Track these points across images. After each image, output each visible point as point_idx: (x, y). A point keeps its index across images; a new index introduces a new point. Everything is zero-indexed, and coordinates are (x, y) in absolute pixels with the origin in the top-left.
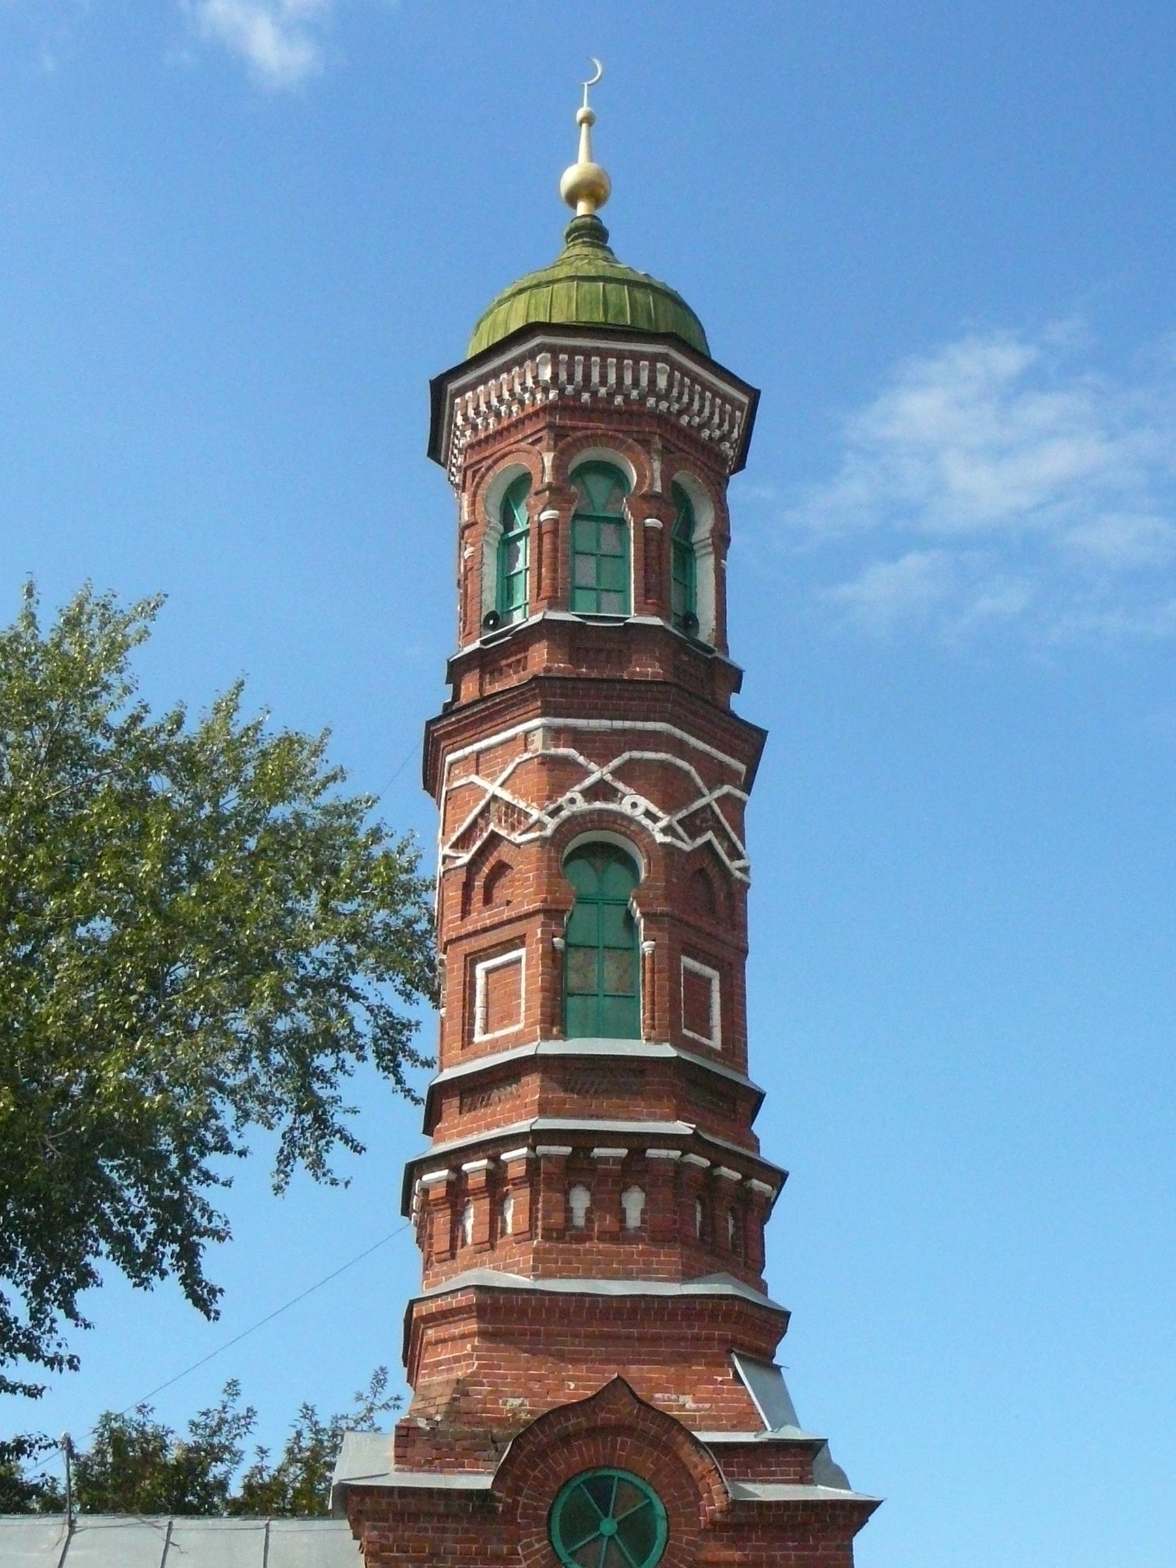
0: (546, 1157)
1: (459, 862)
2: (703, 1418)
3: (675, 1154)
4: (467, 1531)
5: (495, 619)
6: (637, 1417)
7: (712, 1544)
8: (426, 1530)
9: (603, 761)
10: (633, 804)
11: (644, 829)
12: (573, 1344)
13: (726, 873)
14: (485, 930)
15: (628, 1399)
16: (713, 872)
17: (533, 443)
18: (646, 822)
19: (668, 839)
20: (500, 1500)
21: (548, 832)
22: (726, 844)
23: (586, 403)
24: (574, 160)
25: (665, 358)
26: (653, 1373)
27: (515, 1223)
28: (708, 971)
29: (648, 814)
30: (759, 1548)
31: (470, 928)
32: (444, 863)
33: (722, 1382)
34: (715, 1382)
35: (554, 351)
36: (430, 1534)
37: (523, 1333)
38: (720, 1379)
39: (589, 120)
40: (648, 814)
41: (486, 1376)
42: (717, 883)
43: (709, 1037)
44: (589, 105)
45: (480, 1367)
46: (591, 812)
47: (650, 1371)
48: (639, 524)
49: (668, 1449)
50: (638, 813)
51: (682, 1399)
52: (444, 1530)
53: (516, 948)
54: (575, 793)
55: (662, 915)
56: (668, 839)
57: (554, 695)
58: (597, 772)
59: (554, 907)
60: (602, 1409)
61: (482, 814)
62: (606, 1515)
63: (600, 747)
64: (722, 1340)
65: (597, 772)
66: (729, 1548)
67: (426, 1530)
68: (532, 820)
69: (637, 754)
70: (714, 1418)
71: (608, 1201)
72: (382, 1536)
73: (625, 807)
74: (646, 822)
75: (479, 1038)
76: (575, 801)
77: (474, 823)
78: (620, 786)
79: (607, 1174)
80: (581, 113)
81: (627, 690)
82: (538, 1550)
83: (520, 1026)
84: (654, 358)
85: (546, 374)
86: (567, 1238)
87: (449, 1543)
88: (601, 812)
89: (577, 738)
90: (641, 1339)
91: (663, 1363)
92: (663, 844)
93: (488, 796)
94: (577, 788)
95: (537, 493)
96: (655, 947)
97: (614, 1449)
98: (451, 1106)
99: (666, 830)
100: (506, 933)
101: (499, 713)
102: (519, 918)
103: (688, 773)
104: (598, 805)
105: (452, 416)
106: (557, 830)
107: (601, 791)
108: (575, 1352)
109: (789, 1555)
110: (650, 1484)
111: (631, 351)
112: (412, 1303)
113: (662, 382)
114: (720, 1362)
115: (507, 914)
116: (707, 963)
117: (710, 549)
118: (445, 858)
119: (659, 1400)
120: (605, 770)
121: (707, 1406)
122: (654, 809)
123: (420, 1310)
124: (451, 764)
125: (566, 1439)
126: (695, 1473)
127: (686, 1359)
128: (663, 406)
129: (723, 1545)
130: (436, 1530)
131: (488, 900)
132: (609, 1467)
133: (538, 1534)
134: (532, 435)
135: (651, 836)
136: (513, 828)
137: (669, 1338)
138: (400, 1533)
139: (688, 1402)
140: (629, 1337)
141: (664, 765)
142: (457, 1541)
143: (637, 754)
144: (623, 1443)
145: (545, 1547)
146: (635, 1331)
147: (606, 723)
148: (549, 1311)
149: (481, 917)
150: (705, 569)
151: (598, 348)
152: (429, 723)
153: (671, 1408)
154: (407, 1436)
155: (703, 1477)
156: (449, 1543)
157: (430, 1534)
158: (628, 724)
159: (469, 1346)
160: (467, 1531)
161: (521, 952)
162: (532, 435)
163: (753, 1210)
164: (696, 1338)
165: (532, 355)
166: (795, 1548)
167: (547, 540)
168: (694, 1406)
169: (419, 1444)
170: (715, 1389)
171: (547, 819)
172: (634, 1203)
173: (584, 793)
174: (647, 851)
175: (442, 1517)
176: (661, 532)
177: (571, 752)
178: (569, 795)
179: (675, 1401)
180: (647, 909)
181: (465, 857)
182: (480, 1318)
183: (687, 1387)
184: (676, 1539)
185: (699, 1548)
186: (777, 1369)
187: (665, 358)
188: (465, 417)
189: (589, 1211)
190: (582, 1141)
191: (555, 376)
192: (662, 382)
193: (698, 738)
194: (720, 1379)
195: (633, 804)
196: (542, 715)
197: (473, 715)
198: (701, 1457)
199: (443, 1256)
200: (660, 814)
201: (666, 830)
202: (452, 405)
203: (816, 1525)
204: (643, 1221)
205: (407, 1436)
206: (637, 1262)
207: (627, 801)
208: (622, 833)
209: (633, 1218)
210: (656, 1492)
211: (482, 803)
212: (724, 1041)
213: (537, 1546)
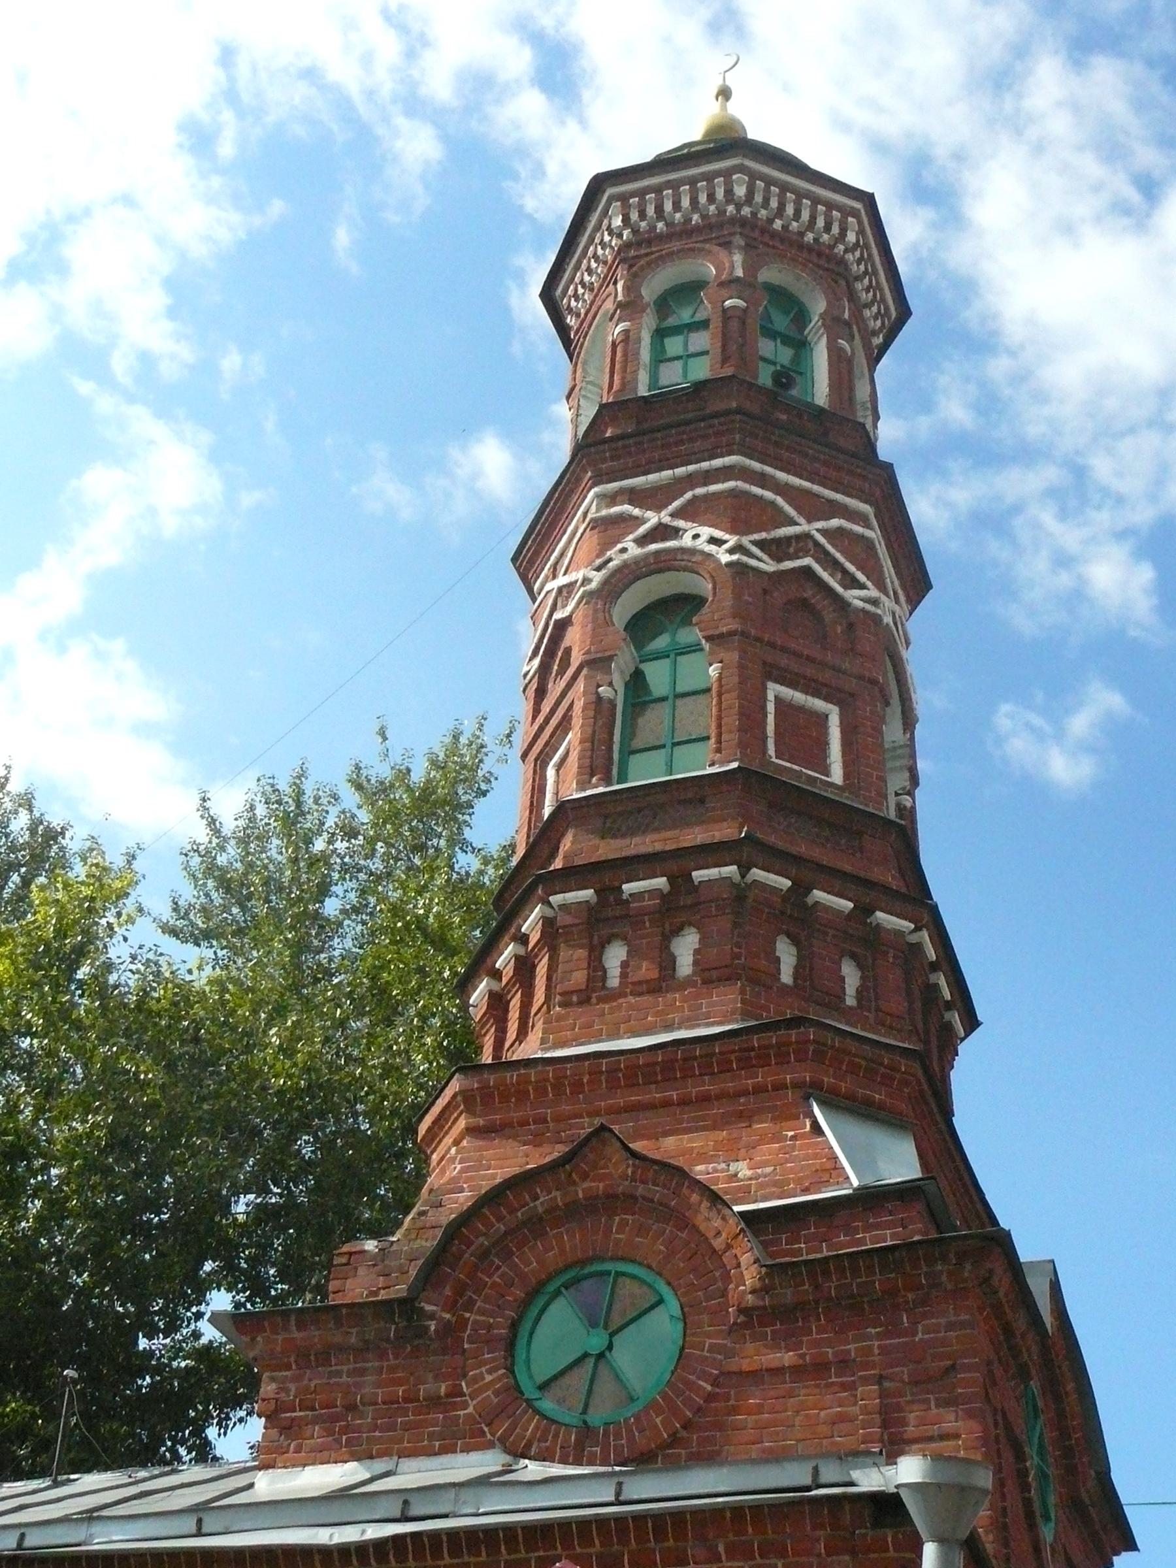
0: (563, 907)
2: (761, 1186)
3: (731, 870)
4: (392, 1369)
6: (633, 1180)
7: (750, 1347)
9: (659, 508)
10: (697, 536)
11: (709, 556)
13: (842, 605)
15: (618, 1155)
16: (818, 601)
18: (712, 549)
20: (432, 1316)
21: (593, 585)
22: (839, 576)
23: (661, 233)
25: (741, 169)
26: (695, 1141)
28: (819, 704)
29: (713, 541)
30: (817, 1344)
33: (793, 1138)
34: (785, 1138)
36: (345, 1379)
37: (523, 1123)
38: (791, 1134)
40: (713, 541)
42: (829, 615)
43: (826, 771)
45: (462, 1171)
46: (646, 556)
47: (691, 1140)
49: (684, 1222)
50: (702, 544)
51: (734, 1167)
52: (362, 1372)
54: (628, 543)
55: (731, 634)
56: (735, 557)
57: (604, 460)
58: (652, 518)
59: (599, 655)
60: (585, 1176)
64: (796, 1085)
65: (652, 518)
66: (776, 1347)
70: (775, 1184)
72: (280, 1390)
73: (686, 541)
78: (681, 523)
79: (642, 912)
81: (684, 433)
84: (727, 174)
85: (740, 191)
86: (594, 1000)
87: (370, 1387)
88: (657, 553)
89: (635, 497)
90: (684, 1102)
91: (714, 1128)
92: (730, 565)
94: (631, 537)
96: (722, 668)
97: (608, 1231)
101: (562, 510)
103: (773, 503)
104: (654, 547)
106: (606, 582)
107: (662, 532)
109: (870, 1347)
110: (660, 1274)
111: (702, 173)
114: (797, 1112)
116: (816, 694)
119: (701, 1173)
120: (663, 514)
121: (769, 1169)
122: (718, 534)
125: (536, 1226)
126: (718, 1243)
127: (746, 1117)
129: (766, 1346)
132: (602, 1259)
133: (493, 1360)
135: (718, 561)
138: (305, 1382)
139: (743, 1169)
140: (667, 1104)
141: (733, 493)
142: (378, 1385)
147: (667, 473)
148: (558, 1087)
151: (669, 181)
152: (514, 560)
153: (716, 1181)
154: (348, 1264)
155: (729, 1247)
156: (370, 1387)
158: (691, 468)
160: (392, 1369)
163: (886, 953)
164: (759, 1090)
167: (619, 349)
168: (749, 1173)
169: (361, 1271)
170: (780, 1149)
173: (636, 541)
174: (712, 577)
175: (360, 1352)
176: (745, 310)
179: (722, 1171)
180: (710, 633)
182: (470, 1110)
183: (743, 1151)
185: (730, 1354)
187: (741, 169)
193: (788, 472)
194: (791, 1134)
195: (697, 536)
196: (595, 485)
198: (724, 1219)
200: (727, 537)
203: (910, 1296)
205: (348, 1264)
208: (685, 569)
209: (685, 965)
210: (669, 1284)
212: (846, 776)
213: (488, 1378)
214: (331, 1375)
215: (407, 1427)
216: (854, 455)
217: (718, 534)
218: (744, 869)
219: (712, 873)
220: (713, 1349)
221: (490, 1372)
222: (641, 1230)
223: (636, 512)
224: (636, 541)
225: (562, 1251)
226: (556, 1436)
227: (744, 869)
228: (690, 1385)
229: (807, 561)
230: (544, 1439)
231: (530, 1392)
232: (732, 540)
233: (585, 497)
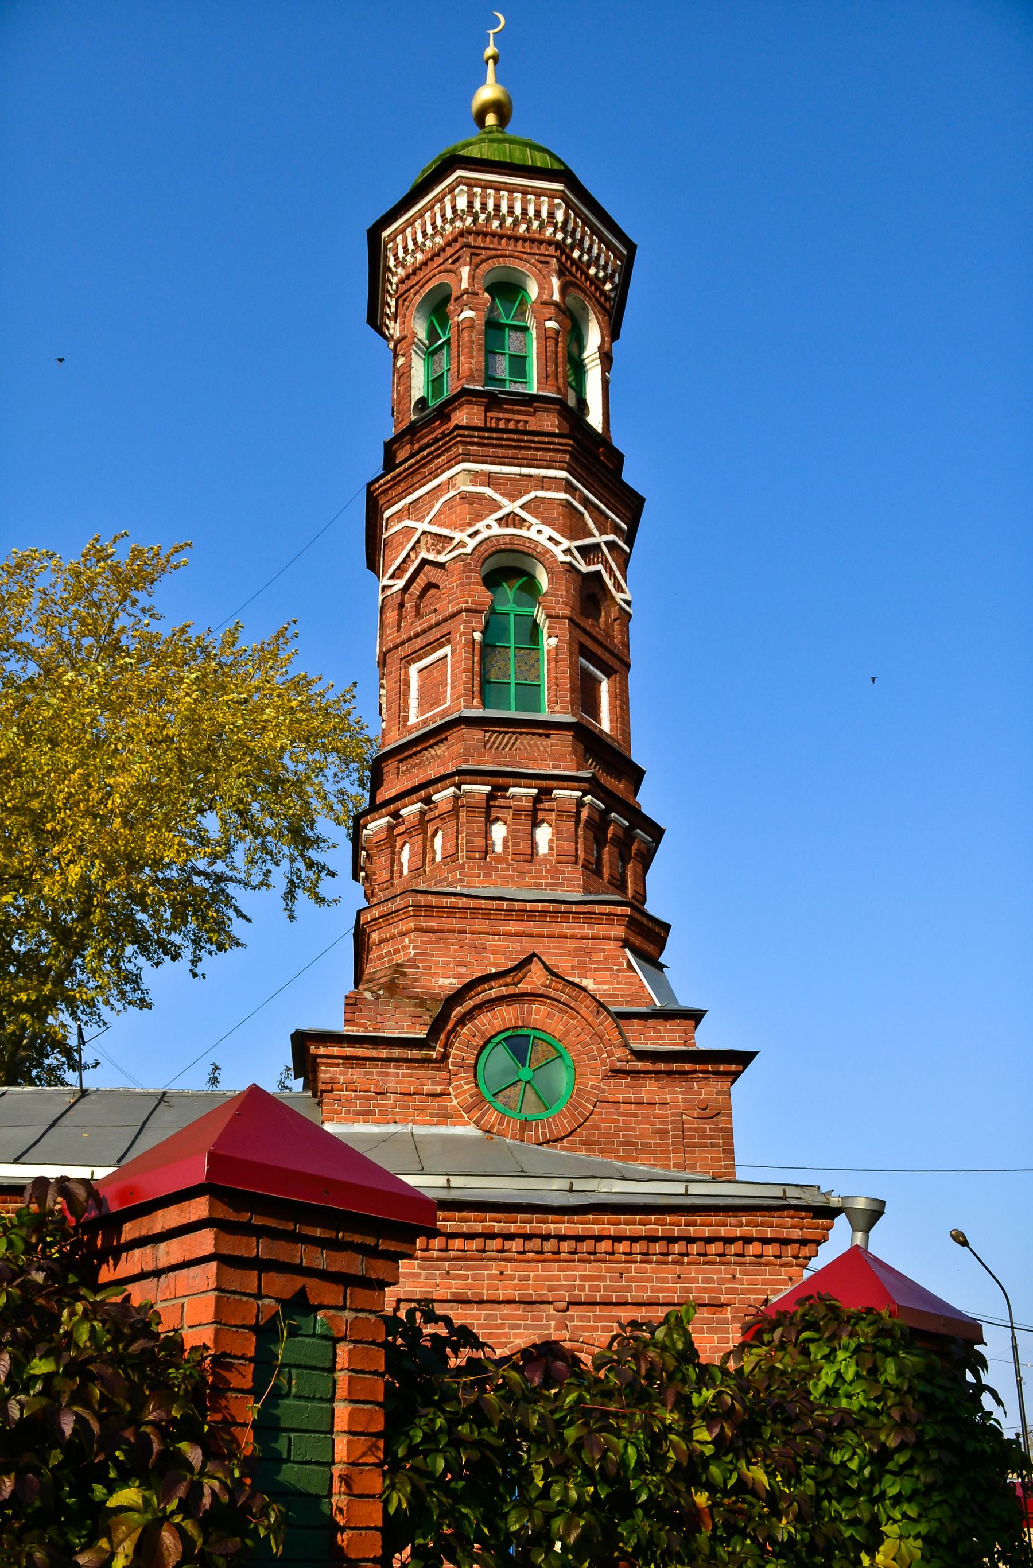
1: (395, 589)
8: (372, 1074)
9: (513, 498)
11: (548, 551)
12: (494, 940)
14: (417, 636)
17: (453, 263)
18: (550, 545)
19: (568, 559)
21: (468, 550)
24: (482, 82)
27: (444, 848)
31: (404, 637)
32: (383, 591)
33: (618, 970)
35: (470, 184)
39: (495, 58)
40: (550, 539)
41: (421, 961)
44: (495, 45)
45: (416, 954)
48: (540, 326)
50: (542, 539)
53: (442, 646)
54: (491, 520)
56: (568, 559)
61: (413, 548)
62: (524, 1065)
63: (513, 488)
65: (509, 507)
67: (372, 1074)
68: (455, 542)
69: (541, 494)
73: (532, 534)
76: (490, 528)
77: (408, 556)
80: (490, 51)
82: (465, 1091)
83: (448, 704)
85: (462, 203)
89: (489, 479)
93: (419, 532)
95: (456, 299)
98: (390, 767)
99: (567, 551)
100: (435, 634)
102: (445, 620)
105: (386, 257)
107: (510, 520)
108: (495, 945)
112: (359, 912)
113: (560, 216)
115: (434, 618)
117: (598, 361)
118: (384, 588)
121: (605, 987)
122: (557, 536)
123: (367, 917)
124: (388, 519)
130: (379, 1074)
131: (418, 614)
134: (451, 256)
135: (553, 556)
136: (439, 552)
137: (572, 937)
143: (541, 494)
144: (538, 1011)
145: (472, 1088)
146: (545, 931)
152: (369, 485)
154: (355, 1004)
157: (375, 1077)
159: (407, 940)
161: (447, 650)
162: (451, 256)
165: (451, 189)
166: (682, 1093)
168: (595, 987)
171: (467, 540)
173: (499, 521)
178: (485, 522)
181: (400, 583)
184: (581, 1083)
186: (661, 967)
188: (396, 258)
189: (505, 839)
191: (470, 205)
192: (560, 216)
194: (616, 967)
195: (539, 532)
197: (405, 470)
199: (385, 885)
201: (567, 551)
202: (386, 249)
204: (551, 848)
206: (546, 878)
211: (414, 539)
213: (466, 1087)
214: (366, 1073)
215: (415, 1108)
216: (458, 372)
217: (557, 536)
218: (458, 786)
219: (567, 793)
220: (593, 1087)
221: (466, 1084)
222: (549, 1016)
223: (497, 497)
224: (499, 521)
225: (503, 1019)
226: (508, 1123)
227: (458, 786)
228: (581, 1105)
229: (599, 567)
230: (501, 1124)
231: (488, 1097)
232: (566, 543)
233: (452, 466)
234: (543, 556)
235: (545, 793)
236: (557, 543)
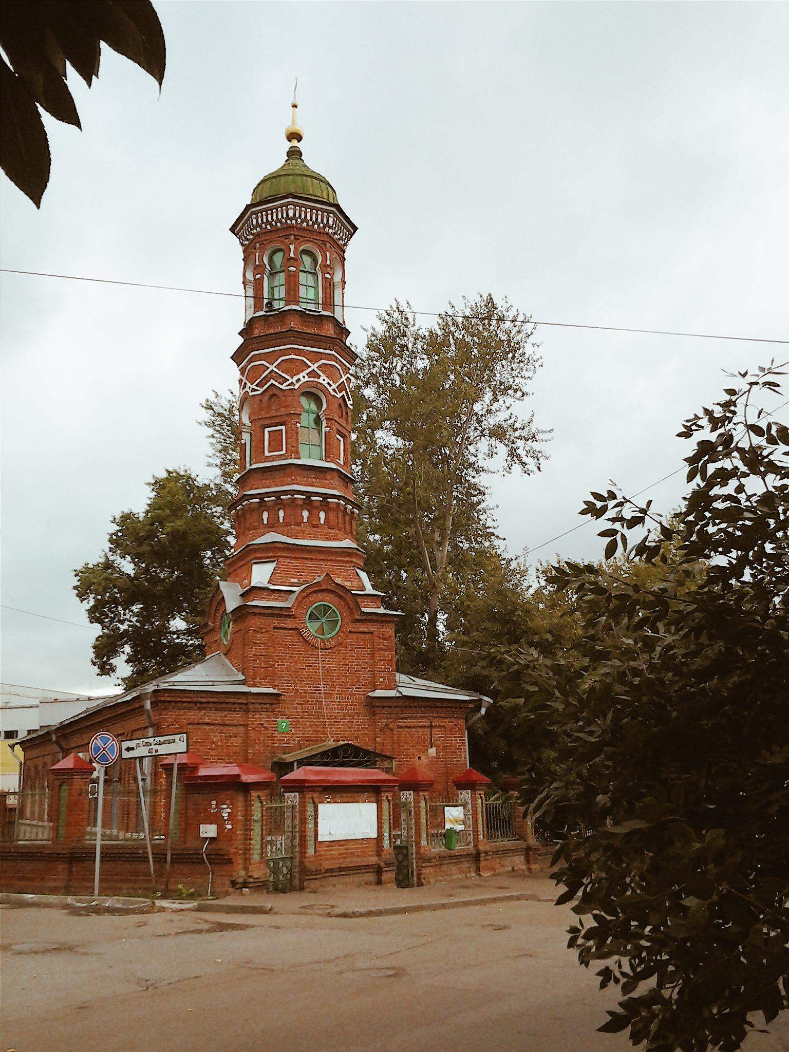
5: (270, 304)
10: (323, 380)
29: (328, 384)
40: (328, 384)
50: (325, 383)
54: (304, 374)
63: (270, 358)
71: (313, 516)
73: (321, 380)
74: (300, 383)
75: (267, 454)
84: (328, 212)
85: (291, 213)
107: (313, 374)
113: (331, 222)
128: (331, 231)
149: (263, 414)
150: (337, 293)
172: (322, 515)
177: (293, 356)
190: (309, 494)
195: (323, 380)
207: (321, 378)
234: (325, 391)
235: (308, 498)
236: (330, 385)
